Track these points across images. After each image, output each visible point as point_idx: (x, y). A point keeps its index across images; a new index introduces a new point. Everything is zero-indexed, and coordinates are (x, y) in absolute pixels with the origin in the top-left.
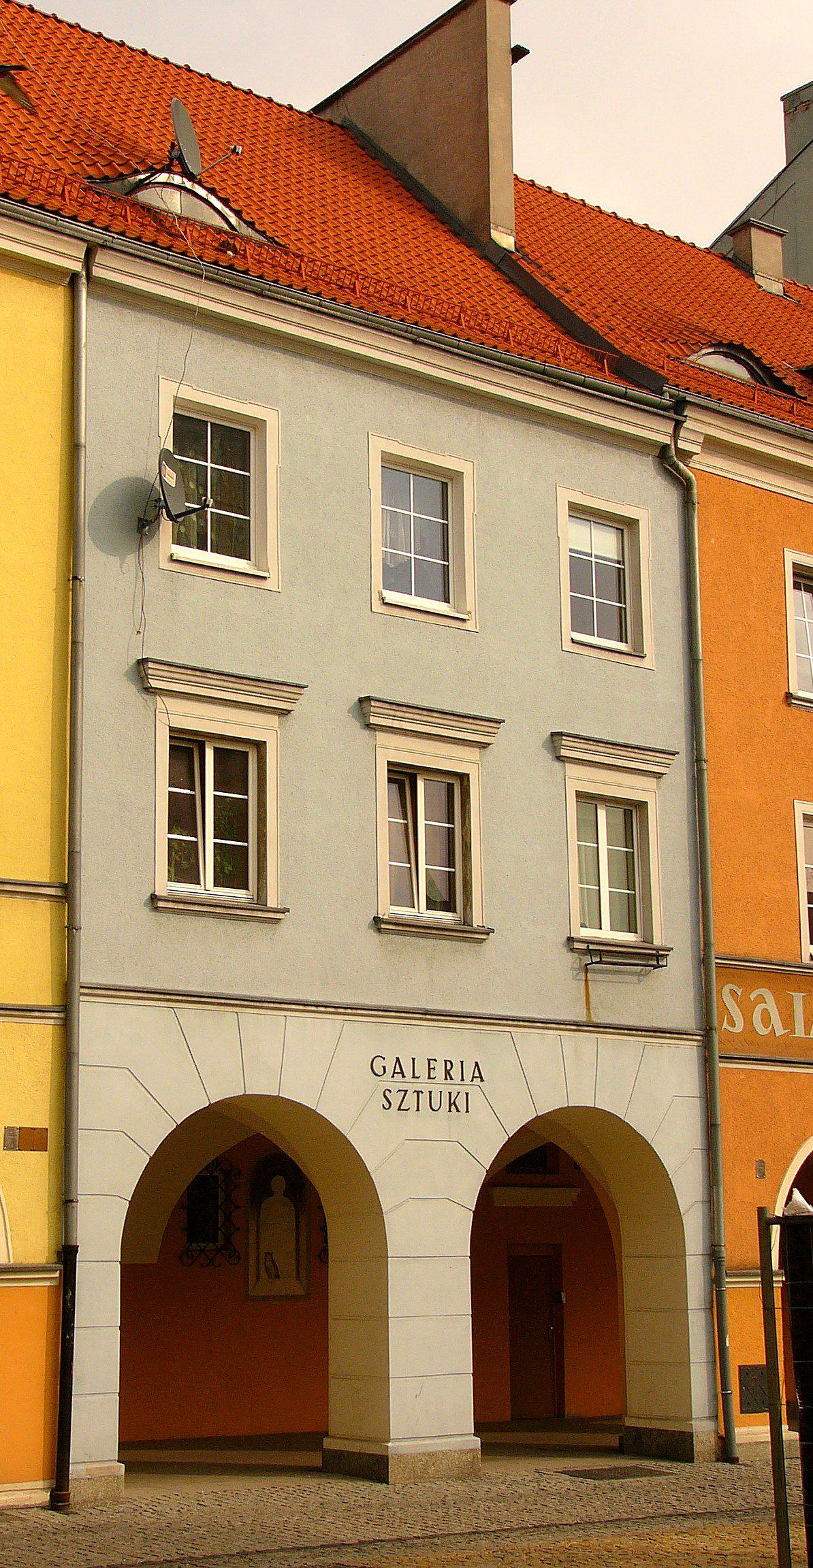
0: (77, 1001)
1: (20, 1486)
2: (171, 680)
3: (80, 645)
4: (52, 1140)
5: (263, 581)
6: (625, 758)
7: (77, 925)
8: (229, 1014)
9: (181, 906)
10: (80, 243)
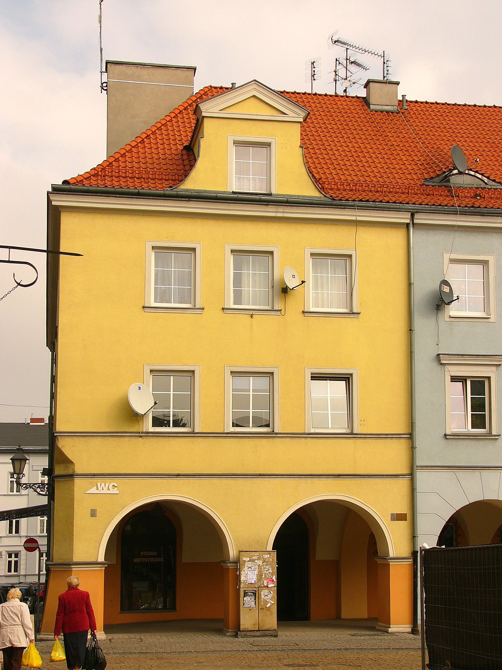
0: (415, 471)
1: (401, 626)
2: (450, 360)
3: (413, 353)
4: (409, 517)
5: (489, 319)
6: (483, 360)
7: (415, 447)
8: (477, 473)
9: (456, 437)
10: (408, 213)
